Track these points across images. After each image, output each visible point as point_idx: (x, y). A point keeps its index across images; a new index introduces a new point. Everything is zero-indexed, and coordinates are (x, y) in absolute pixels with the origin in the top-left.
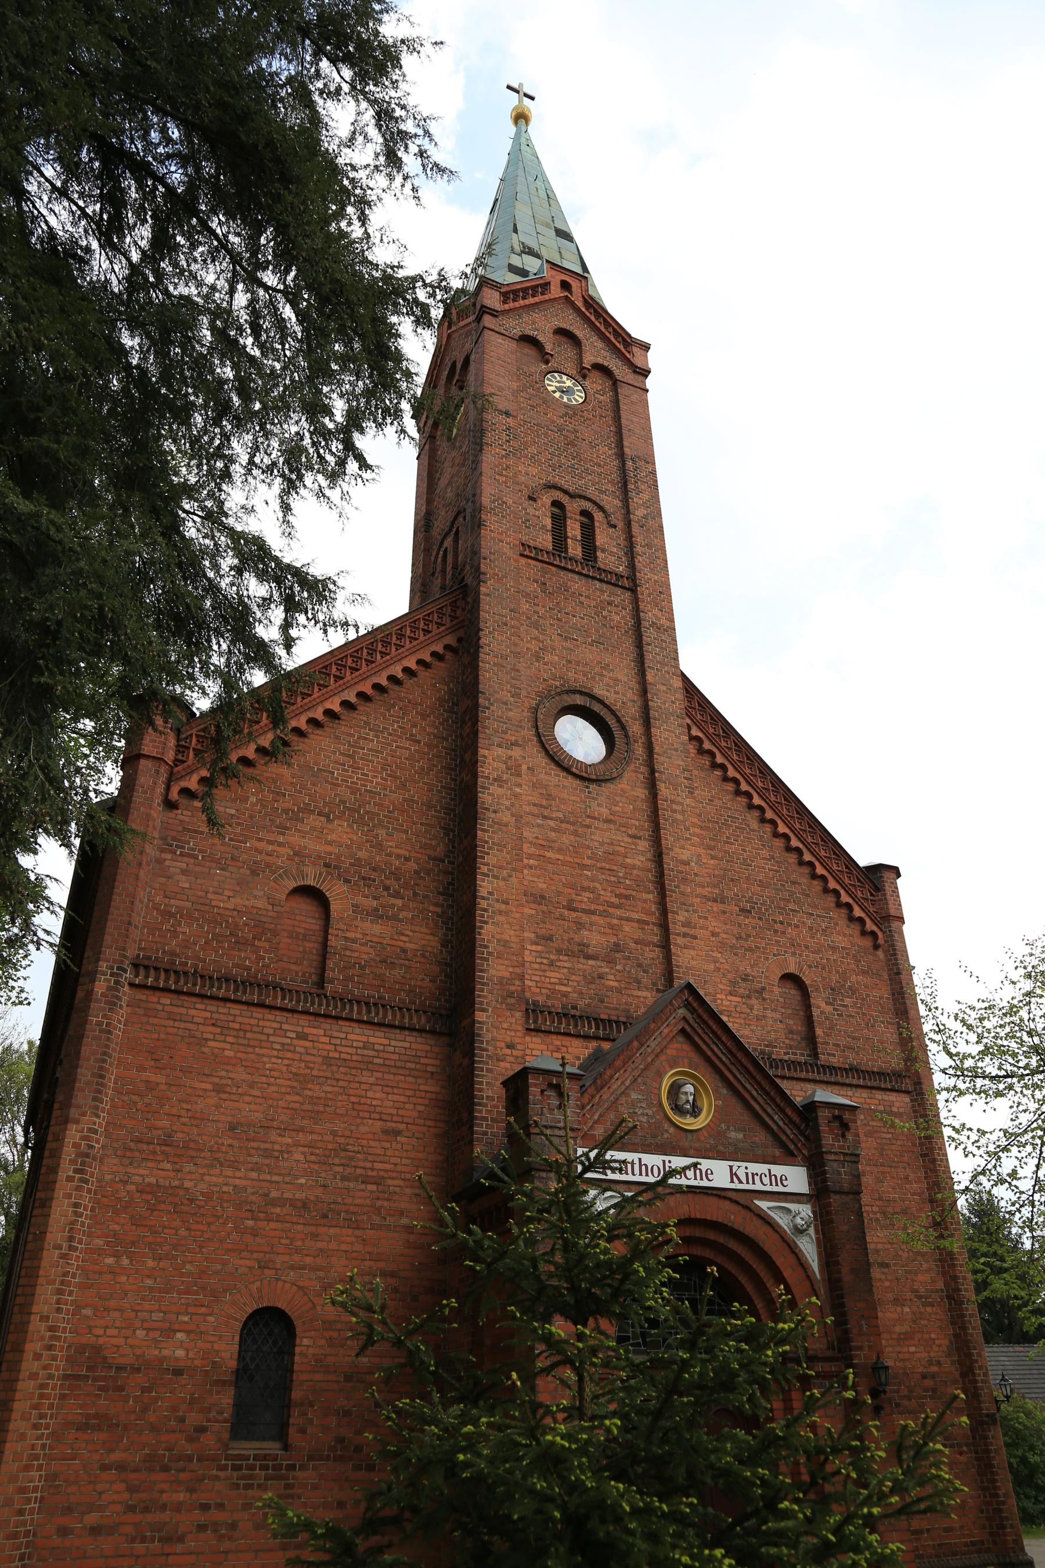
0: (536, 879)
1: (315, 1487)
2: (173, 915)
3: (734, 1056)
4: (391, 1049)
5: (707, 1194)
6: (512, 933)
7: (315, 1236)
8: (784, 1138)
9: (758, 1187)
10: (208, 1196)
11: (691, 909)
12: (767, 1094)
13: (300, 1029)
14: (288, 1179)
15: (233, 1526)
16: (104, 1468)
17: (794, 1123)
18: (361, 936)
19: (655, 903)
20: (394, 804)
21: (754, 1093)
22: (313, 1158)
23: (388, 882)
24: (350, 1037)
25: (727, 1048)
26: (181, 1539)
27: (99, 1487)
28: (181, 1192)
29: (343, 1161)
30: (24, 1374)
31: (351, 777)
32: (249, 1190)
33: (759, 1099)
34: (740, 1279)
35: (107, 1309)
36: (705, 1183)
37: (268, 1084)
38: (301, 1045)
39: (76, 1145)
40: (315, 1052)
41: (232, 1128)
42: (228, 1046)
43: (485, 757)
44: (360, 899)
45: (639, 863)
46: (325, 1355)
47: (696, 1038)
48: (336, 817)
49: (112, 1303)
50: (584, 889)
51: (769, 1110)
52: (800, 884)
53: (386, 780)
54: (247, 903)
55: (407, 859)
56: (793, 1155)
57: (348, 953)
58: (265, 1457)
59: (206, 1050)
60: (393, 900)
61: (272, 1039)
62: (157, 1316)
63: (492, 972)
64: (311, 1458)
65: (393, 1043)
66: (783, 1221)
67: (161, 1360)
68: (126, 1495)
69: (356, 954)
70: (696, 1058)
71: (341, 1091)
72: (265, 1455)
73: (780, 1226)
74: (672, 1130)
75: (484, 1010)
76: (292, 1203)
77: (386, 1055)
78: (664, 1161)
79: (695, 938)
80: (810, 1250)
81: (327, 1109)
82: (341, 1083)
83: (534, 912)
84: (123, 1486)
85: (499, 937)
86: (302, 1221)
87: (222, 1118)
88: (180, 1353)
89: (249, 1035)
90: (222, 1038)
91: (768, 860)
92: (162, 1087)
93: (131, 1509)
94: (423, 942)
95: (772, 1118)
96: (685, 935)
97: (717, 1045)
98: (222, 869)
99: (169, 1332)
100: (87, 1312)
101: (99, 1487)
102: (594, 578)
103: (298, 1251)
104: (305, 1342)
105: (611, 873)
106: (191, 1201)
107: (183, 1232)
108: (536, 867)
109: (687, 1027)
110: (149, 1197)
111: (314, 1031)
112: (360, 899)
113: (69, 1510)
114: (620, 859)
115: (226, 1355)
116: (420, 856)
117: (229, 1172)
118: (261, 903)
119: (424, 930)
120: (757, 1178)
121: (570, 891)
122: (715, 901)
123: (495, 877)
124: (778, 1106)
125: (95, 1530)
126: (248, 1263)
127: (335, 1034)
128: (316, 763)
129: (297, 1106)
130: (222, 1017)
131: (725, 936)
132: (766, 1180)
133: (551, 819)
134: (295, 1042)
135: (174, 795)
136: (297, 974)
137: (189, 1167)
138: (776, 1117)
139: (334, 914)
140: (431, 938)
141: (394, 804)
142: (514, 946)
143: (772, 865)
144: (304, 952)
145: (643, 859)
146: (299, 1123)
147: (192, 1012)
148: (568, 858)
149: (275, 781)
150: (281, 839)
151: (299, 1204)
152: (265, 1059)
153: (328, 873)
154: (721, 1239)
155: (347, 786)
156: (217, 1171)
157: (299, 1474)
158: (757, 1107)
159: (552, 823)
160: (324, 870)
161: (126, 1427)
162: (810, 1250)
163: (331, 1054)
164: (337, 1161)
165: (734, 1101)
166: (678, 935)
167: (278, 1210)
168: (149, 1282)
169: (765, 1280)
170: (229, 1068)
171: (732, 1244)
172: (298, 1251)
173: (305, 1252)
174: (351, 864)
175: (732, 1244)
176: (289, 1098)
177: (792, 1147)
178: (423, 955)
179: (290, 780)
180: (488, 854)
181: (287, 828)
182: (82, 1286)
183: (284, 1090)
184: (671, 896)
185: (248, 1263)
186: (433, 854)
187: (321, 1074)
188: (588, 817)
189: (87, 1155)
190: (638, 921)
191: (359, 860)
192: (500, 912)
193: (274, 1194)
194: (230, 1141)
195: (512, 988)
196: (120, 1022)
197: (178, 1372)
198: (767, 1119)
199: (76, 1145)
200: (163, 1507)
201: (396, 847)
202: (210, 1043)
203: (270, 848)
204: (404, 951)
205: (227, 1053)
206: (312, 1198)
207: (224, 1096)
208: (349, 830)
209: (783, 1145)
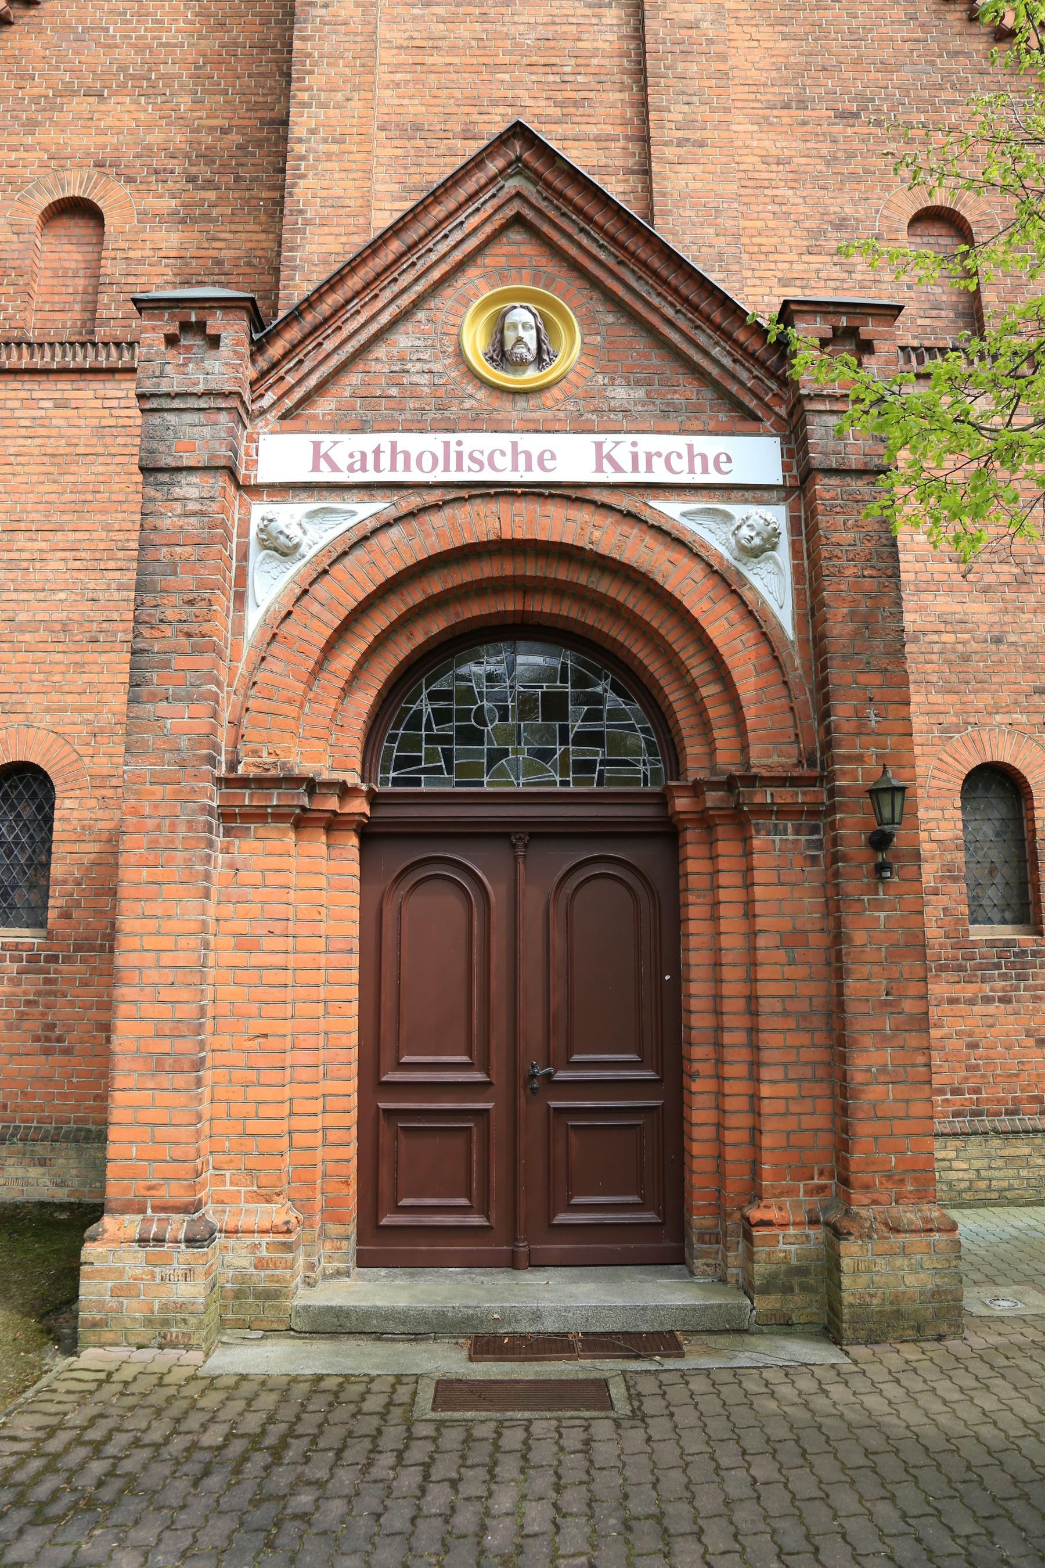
0: (406, 102)
1: (85, 983)
3: (622, 246)
5: (540, 495)
6: (351, 184)
7: (80, 668)
8: (734, 388)
9: (660, 476)
11: (695, 99)
12: (695, 308)
13: (58, 395)
14: (41, 595)
17: (751, 355)
18: (151, 253)
19: (632, 105)
20: (204, 55)
21: (669, 312)
22: (78, 564)
23: (194, 170)
25: (606, 233)
29: (120, 564)
31: (135, 30)
33: (681, 322)
34: (634, 650)
37: (14, 474)
38: (59, 417)
40: (82, 422)
44: (151, 203)
45: (606, 45)
46: (96, 820)
47: (546, 228)
48: (115, 93)
50: (494, 103)
51: (701, 339)
52: (968, 55)
53: (192, 23)
55: (224, 131)
56: (757, 419)
58: (17, 947)
60: (202, 194)
61: (17, 413)
63: (308, 248)
64: (78, 948)
69: (143, 279)
70: (550, 267)
71: (118, 469)
72: (17, 943)
73: (705, 546)
74: (481, 394)
76: (47, 626)
78: (447, 445)
79: (701, 144)
80: (774, 588)
81: (98, 496)
82: (119, 459)
83: (400, 152)
85: (324, 193)
91: (900, 22)
94: (249, 245)
95: (706, 353)
96: (681, 143)
97: (588, 234)
103: (58, 688)
104: (68, 804)
105: (548, 69)
108: (407, 82)
109: (529, 214)
112: (151, 203)
114: (569, 45)
116: (246, 122)
119: (251, 227)
120: (658, 463)
121: (467, 109)
122: (787, 106)
123: (323, 106)
124: (717, 328)
128: (80, 21)
131: (803, 161)
132: (680, 464)
136: (64, 323)
138: (716, 352)
140: (263, 236)
141: (204, 55)
142: (352, 203)
143: (909, 31)
145: (610, 37)
146: (57, 518)
148: (465, 60)
149: (17, 60)
150: (29, 140)
152: (8, 442)
153: (99, 178)
154: (582, 578)
155: (130, 45)
157: (62, 967)
158: (674, 337)
160: (95, 172)
162: (774, 588)
163: (104, 422)
164: (111, 565)
165: (628, 333)
166: (666, 144)
167: (27, 637)
169: (676, 647)
171: (606, 586)
172: (58, 688)
173: (66, 688)
174: (137, 156)
175: (606, 586)
177: (752, 404)
178: (249, 264)
179: (41, 53)
180: (311, 72)
181: (37, 124)
183: (34, 479)
184: (657, 85)
186: (268, 115)
187: (89, 450)
190: (597, 138)
191: (149, 147)
192: (329, 157)
193: (22, 617)
198: (697, 357)
201: (208, 117)
204: (219, 262)
206: (76, 617)
208: (133, 107)
209: (737, 405)
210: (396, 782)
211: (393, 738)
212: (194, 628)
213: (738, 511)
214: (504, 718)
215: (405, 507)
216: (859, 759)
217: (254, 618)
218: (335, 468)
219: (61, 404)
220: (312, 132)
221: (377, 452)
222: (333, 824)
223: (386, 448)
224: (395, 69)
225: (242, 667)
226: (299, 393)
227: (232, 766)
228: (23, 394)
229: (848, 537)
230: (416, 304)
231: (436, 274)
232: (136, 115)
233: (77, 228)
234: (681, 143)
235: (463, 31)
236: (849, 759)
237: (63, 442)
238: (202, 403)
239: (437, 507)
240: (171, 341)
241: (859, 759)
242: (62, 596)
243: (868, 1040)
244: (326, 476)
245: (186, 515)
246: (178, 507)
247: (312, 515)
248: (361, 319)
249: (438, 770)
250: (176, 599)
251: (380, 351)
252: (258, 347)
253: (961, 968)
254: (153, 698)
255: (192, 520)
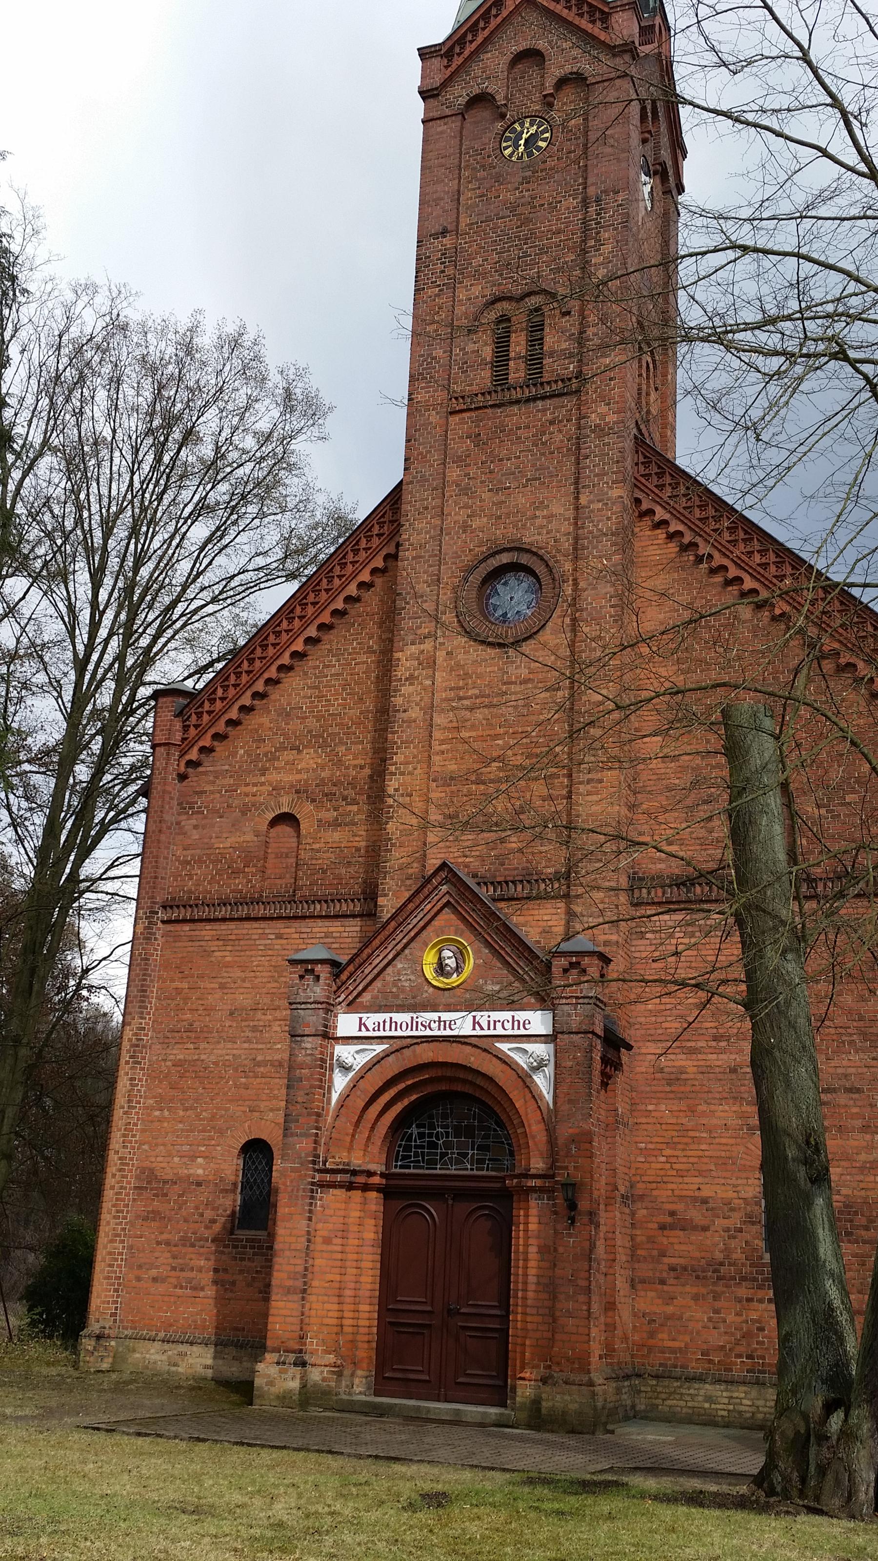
2: (189, 863)
4: (346, 934)
9: (500, 1031)
10: (216, 1063)
14: (269, 1046)
15: (233, 1283)
16: (159, 1243)
23: (346, 793)
24: (314, 930)
26: (202, 1289)
27: (157, 1254)
28: (199, 1063)
30: (107, 1186)
32: (243, 1057)
35: (157, 1145)
36: (448, 1032)
39: (130, 1040)
41: (231, 1014)
42: (228, 953)
43: (399, 660)
48: (305, 747)
49: (160, 1140)
54: (238, 840)
55: (362, 767)
57: (314, 862)
58: (253, 1241)
59: (213, 959)
60: (349, 808)
61: (258, 942)
62: (186, 1148)
65: (347, 929)
66: (520, 1060)
67: (189, 1176)
68: (171, 1260)
69: (320, 861)
74: (431, 989)
75: (386, 895)
76: (272, 1063)
77: (342, 940)
79: (601, 781)
83: (443, 794)
84: (169, 1255)
86: (278, 1075)
87: (225, 1007)
88: (200, 1172)
89: (242, 943)
90: (223, 948)
92: (186, 991)
93: (174, 1269)
96: (589, 781)
98: (221, 817)
99: (193, 1158)
100: (146, 1147)
101: (157, 1254)
102: (535, 399)
106: (205, 1068)
107: (200, 1090)
110: (179, 1068)
111: (287, 930)
113: (140, 1267)
115: (228, 1172)
117: (229, 1045)
118: (250, 837)
120: (499, 1025)
125: (155, 1280)
126: (243, 1108)
127: (303, 930)
129: (274, 990)
130: (224, 932)
132: (508, 1026)
133: (466, 698)
134: (275, 942)
135: (182, 769)
137: (203, 1045)
139: (303, 832)
144: (287, 867)
146: (277, 1003)
147: (204, 933)
149: (257, 731)
151: (277, 1063)
153: (299, 798)
156: (222, 1045)
159: (466, 702)
160: (295, 796)
161: (170, 1220)
167: (262, 1069)
168: (181, 1126)
170: (229, 969)
171: (479, 1081)
176: (269, 985)
180: (396, 754)
182: (143, 1131)
185: (243, 1108)
188: (505, 684)
189: (137, 1046)
193: (259, 1058)
194: (230, 1023)
195: (410, 871)
196: (156, 950)
197: (199, 1184)
199: (130, 1040)
200: (192, 1269)
202: (217, 954)
203: (255, 789)
205: (228, 959)
207: (225, 991)
210: (401, 1167)
211: (400, 1146)
212: (309, 1106)
213: (529, 1047)
214: (447, 1137)
215: (395, 1047)
216: (566, 1168)
217: (335, 1097)
218: (368, 1030)
219: (279, 936)
220: (396, 790)
221: (384, 1022)
222: (366, 1188)
223: (388, 1020)
224: (442, 742)
225: (329, 1119)
226: (355, 993)
227: (324, 1163)
228: (260, 931)
229: (570, 1064)
230: (405, 947)
231: (412, 934)
232: (316, 760)
233: (285, 830)
234: (589, 781)
235: (479, 715)
236: (561, 1168)
237: (280, 958)
238: (313, 1006)
239: (408, 1047)
240: (301, 977)
241: (566, 1168)
242: (279, 1046)
243: (562, 1297)
244: (364, 1033)
245: (307, 1055)
246: (303, 1052)
247: (358, 1052)
248: (380, 958)
249: (419, 1161)
250: (302, 1093)
251: (390, 970)
252: (337, 976)
253: (755, 1280)
254: (292, 1135)
255: (309, 1058)
